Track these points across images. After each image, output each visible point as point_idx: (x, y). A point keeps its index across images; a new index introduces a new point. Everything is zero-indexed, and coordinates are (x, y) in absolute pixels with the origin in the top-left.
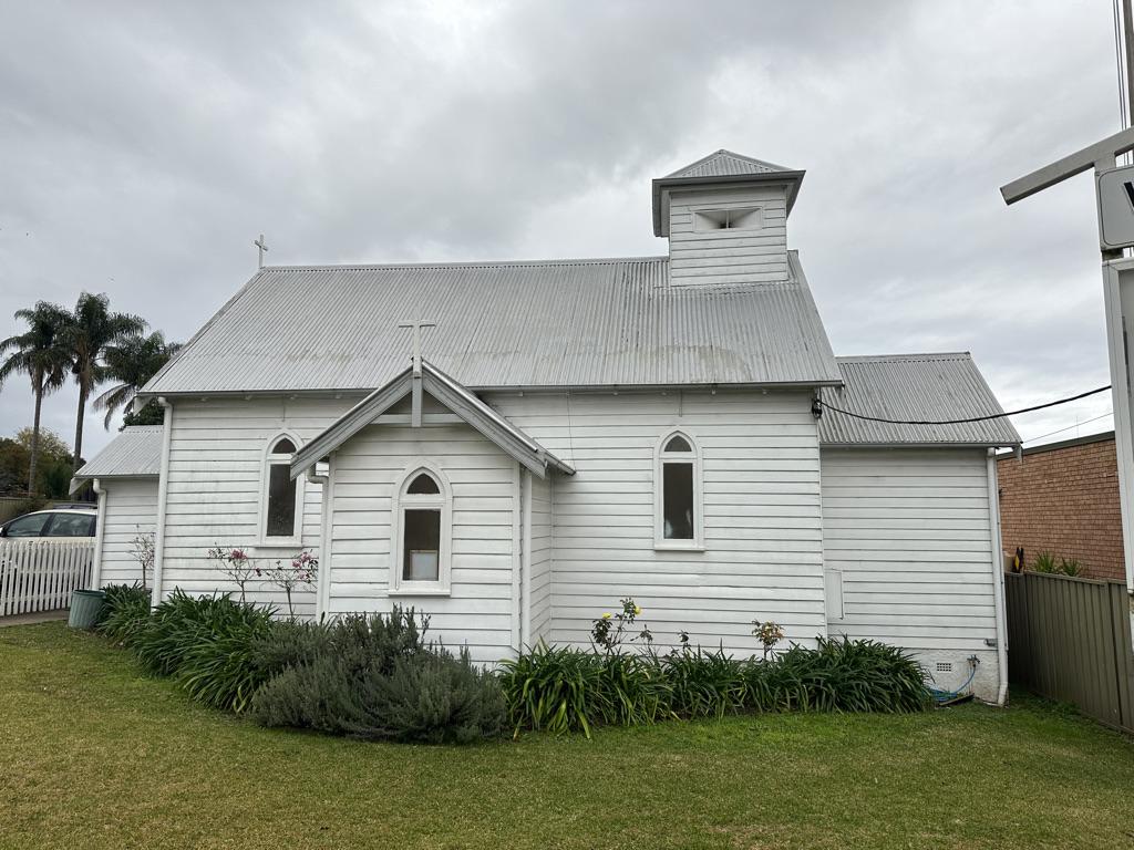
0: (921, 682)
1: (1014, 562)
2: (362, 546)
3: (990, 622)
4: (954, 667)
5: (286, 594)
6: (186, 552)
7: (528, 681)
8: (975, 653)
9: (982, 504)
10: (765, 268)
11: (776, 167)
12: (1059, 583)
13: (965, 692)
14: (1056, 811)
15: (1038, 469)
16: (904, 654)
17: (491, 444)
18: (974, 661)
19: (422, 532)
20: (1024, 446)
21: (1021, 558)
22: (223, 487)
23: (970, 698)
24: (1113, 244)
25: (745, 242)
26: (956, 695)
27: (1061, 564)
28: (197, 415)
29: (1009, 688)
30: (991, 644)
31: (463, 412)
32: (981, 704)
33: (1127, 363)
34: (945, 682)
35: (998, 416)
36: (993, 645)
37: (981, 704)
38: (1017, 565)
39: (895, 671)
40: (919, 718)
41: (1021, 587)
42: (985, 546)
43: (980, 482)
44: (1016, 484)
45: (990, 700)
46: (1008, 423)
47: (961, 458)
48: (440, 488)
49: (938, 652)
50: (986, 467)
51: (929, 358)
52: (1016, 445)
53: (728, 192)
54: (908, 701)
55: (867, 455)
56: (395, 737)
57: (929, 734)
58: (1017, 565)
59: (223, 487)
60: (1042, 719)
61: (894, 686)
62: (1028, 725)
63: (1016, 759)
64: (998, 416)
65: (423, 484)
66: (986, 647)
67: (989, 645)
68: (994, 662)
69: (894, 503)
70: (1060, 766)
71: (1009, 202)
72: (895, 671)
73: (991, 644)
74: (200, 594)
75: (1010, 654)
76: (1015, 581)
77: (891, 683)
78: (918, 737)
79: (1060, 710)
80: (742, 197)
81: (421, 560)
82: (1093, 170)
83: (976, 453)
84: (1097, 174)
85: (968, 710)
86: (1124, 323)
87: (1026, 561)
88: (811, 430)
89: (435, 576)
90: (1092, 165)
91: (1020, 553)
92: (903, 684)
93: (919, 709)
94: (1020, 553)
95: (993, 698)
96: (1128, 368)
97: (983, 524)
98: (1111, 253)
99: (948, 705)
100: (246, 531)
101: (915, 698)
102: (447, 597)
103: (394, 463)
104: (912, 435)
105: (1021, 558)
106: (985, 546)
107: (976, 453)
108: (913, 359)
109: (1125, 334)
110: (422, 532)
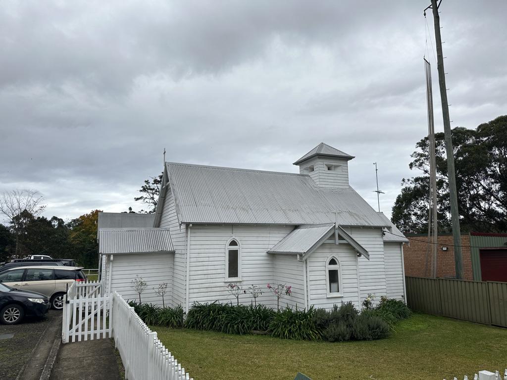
2: (318, 282)
6: (197, 286)
7: (229, 325)
10: (343, 184)
11: (346, 154)
17: (354, 248)
19: (333, 276)
22: (211, 259)
25: (339, 176)
28: (200, 231)
31: (348, 240)
41: (409, 279)
48: (338, 263)
50: (401, 248)
53: (336, 159)
59: (211, 259)
65: (333, 262)
74: (204, 303)
80: (339, 162)
81: (334, 285)
88: (381, 239)
89: (337, 290)
100: (221, 276)
102: (342, 297)
103: (325, 255)
110: (333, 276)
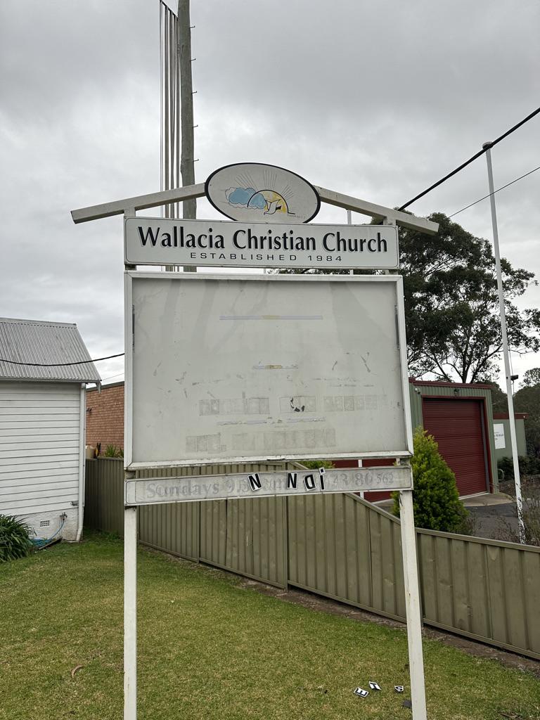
0: (27, 537)
1: (95, 451)
3: (75, 491)
4: (52, 523)
5: (301, 398)
8: (63, 511)
9: (76, 417)
12: (115, 462)
13: (57, 537)
14: (96, 603)
15: (112, 396)
16: (17, 520)
18: (63, 517)
20: (103, 383)
21: (99, 450)
23: (59, 541)
24: (131, 261)
26: (51, 540)
27: (119, 451)
29: (84, 529)
30: (75, 504)
32: (66, 543)
33: (133, 333)
34: (41, 533)
35: (70, 364)
36: (76, 505)
37: (65, 543)
38: (97, 454)
39: (9, 533)
40: (22, 562)
42: (75, 444)
43: (75, 404)
44: (99, 405)
45: (70, 539)
46: (93, 366)
47: (64, 389)
49: (41, 514)
50: (80, 395)
51: (51, 325)
52: (98, 382)
54: (17, 551)
55: (51, 389)
56: (279, 432)
57: (26, 572)
58: (97, 454)
60: (100, 544)
61: (7, 543)
62: (91, 551)
63: (79, 575)
64: (70, 364)
66: (72, 507)
67: (73, 505)
68: (75, 516)
69: (20, 418)
70: (103, 573)
71: (76, 222)
72: (9, 533)
73: (75, 504)
75: (85, 509)
76: (92, 463)
77: (5, 541)
78: (19, 576)
79: (110, 538)
82: (123, 214)
83: (74, 386)
84: (125, 217)
85: (57, 548)
86: (133, 310)
87: (101, 451)
90: (122, 212)
91: (99, 446)
92: (14, 541)
93: (24, 555)
94: (99, 446)
95: (74, 537)
96: (134, 336)
97: (75, 430)
98: (131, 266)
99: (45, 548)
101: (22, 548)
104: (34, 373)
105: (99, 450)
106: (75, 444)
107: (74, 386)
108: (41, 324)
109: (133, 315)
